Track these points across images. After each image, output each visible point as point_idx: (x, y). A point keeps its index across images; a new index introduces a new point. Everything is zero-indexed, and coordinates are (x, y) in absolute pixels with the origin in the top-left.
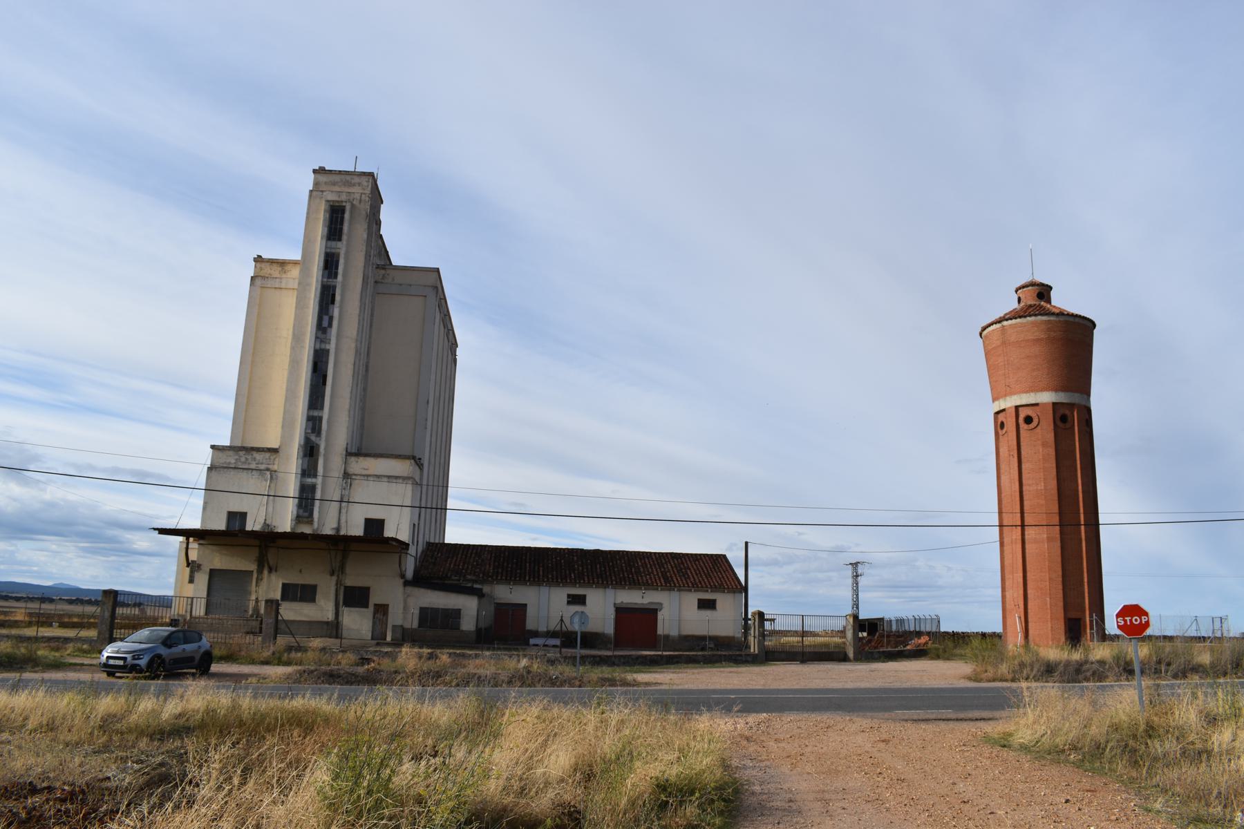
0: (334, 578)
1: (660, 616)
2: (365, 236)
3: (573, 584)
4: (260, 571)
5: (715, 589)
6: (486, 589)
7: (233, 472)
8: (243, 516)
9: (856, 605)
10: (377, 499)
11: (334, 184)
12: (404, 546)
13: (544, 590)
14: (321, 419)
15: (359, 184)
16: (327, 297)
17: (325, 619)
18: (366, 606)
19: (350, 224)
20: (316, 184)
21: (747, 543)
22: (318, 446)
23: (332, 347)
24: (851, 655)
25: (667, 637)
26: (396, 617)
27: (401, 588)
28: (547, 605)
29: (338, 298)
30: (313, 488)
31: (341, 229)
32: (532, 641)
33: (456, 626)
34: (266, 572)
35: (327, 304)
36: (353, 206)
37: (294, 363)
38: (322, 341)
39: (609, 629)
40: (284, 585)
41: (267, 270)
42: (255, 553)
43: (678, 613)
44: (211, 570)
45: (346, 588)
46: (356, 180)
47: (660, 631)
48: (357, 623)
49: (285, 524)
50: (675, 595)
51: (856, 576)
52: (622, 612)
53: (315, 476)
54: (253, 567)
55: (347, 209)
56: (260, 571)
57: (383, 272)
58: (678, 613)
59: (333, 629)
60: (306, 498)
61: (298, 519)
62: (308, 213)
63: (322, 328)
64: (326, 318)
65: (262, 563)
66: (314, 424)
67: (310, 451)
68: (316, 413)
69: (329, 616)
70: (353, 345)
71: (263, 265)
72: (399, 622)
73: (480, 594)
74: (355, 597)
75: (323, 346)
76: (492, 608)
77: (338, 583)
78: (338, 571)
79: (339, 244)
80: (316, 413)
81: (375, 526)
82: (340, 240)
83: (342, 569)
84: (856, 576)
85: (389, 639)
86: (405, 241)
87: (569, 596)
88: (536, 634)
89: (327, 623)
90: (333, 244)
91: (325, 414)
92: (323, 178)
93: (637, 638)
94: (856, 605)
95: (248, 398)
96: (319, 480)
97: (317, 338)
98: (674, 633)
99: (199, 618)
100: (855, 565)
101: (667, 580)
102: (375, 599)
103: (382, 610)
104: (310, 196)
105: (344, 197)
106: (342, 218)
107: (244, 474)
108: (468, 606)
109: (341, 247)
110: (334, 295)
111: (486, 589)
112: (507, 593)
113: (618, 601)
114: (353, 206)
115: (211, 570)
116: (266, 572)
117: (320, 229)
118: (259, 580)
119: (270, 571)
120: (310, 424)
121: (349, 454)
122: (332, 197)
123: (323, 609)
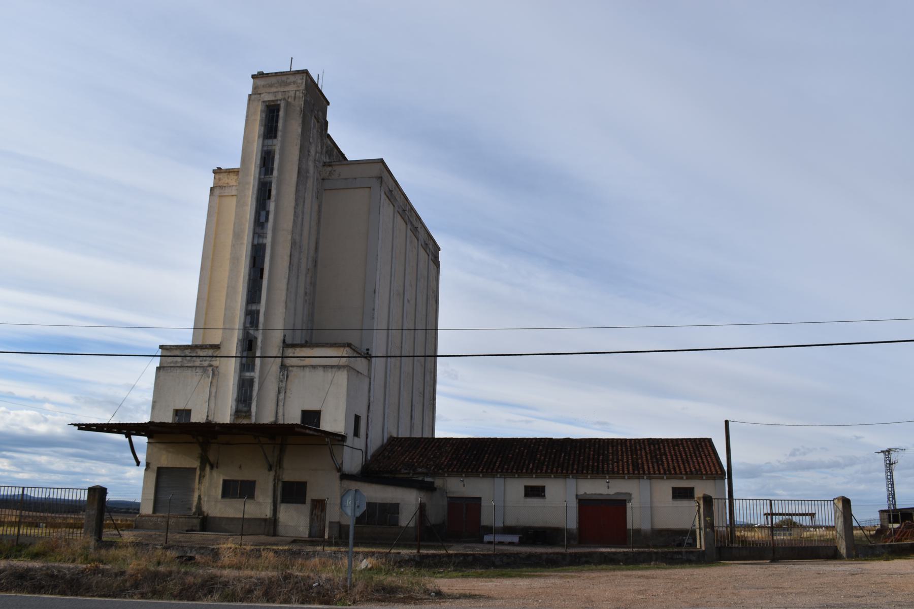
0: (272, 473)
1: (629, 505)
2: (300, 131)
3: (529, 474)
4: (202, 469)
5: (691, 475)
6: (438, 482)
7: (178, 371)
8: (188, 412)
9: (892, 495)
10: (324, 394)
11: (271, 86)
12: (339, 439)
13: (499, 482)
14: (258, 312)
15: (294, 82)
16: (264, 193)
17: (263, 516)
18: (304, 502)
19: (285, 121)
20: (255, 88)
21: (727, 422)
22: (256, 338)
23: (268, 241)
24: (843, 551)
25: (638, 532)
26: (332, 514)
27: (338, 481)
28: (504, 500)
29: (274, 192)
30: (251, 381)
31: (276, 127)
32: (487, 538)
33: (395, 523)
34: (208, 468)
35: (264, 200)
36: (288, 104)
37: (235, 260)
38: (259, 236)
39: (572, 523)
40: (225, 482)
41: (225, 180)
42: (198, 450)
43: (652, 504)
44: (159, 468)
45: (284, 483)
46: (292, 79)
47: (629, 526)
48: (295, 520)
49: (225, 416)
50: (645, 483)
51: (890, 465)
52: (585, 505)
53: (253, 370)
54: (196, 464)
55: (289, 109)
56: (202, 469)
57: (329, 169)
58: (652, 504)
59: (271, 526)
60: (412, 427)
61: (237, 413)
62: (247, 116)
63: (260, 223)
64: (263, 213)
65: (205, 461)
66: (252, 317)
67: (248, 345)
68: (254, 307)
69: (267, 512)
70: (289, 237)
71: (221, 176)
72: (336, 519)
73: (428, 488)
74: (293, 493)
75: (261, 241)
76: (445, 503)
77: (276, 479)
78: (275, 466)
79: (275, 141)
80: (254, 307)
81: (311, 417)
82: (275, 137)
83: (280, 463)
84: (890, 465)
85: (326, 537)
86: (352, 140)
87: (526, 488)
88: (489, 530)
89: (265, 520)
90: (270, 142)
91: (262, 308)
92: (261, 82)
93: (602, 538)
94: (892, 495)
95: (208, 301)
96: (256, 374)
97: (254, 233)
98: (646, 526)
99: (149, 516)
100: (888, 452)
101: (636, 467)
102: (312, 494)
103: (319, 506)
104: (249, 100)
105: (279, 97)
106: (278, 116)
107: (189, 372)
108: (408, 500)
109: (276, 145)
110: (270, 191)
111: (438, 482)
112: (460, 486)
113: (581, 492)
114: (288, 104)
115: (159, 468)
116: (208, 468)
117: (257, 129)
118: (202, 477)
119: (212, 467)
120: (249, 317)
121: (286, 345)
122: (268, 97)
123: (260, 506)
